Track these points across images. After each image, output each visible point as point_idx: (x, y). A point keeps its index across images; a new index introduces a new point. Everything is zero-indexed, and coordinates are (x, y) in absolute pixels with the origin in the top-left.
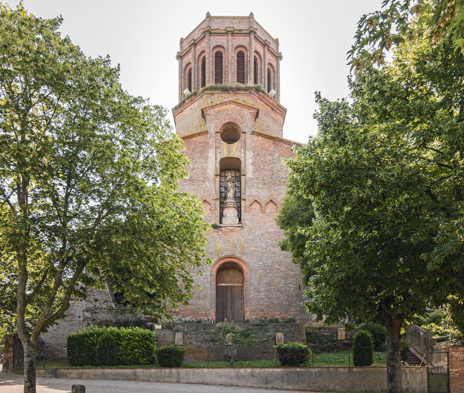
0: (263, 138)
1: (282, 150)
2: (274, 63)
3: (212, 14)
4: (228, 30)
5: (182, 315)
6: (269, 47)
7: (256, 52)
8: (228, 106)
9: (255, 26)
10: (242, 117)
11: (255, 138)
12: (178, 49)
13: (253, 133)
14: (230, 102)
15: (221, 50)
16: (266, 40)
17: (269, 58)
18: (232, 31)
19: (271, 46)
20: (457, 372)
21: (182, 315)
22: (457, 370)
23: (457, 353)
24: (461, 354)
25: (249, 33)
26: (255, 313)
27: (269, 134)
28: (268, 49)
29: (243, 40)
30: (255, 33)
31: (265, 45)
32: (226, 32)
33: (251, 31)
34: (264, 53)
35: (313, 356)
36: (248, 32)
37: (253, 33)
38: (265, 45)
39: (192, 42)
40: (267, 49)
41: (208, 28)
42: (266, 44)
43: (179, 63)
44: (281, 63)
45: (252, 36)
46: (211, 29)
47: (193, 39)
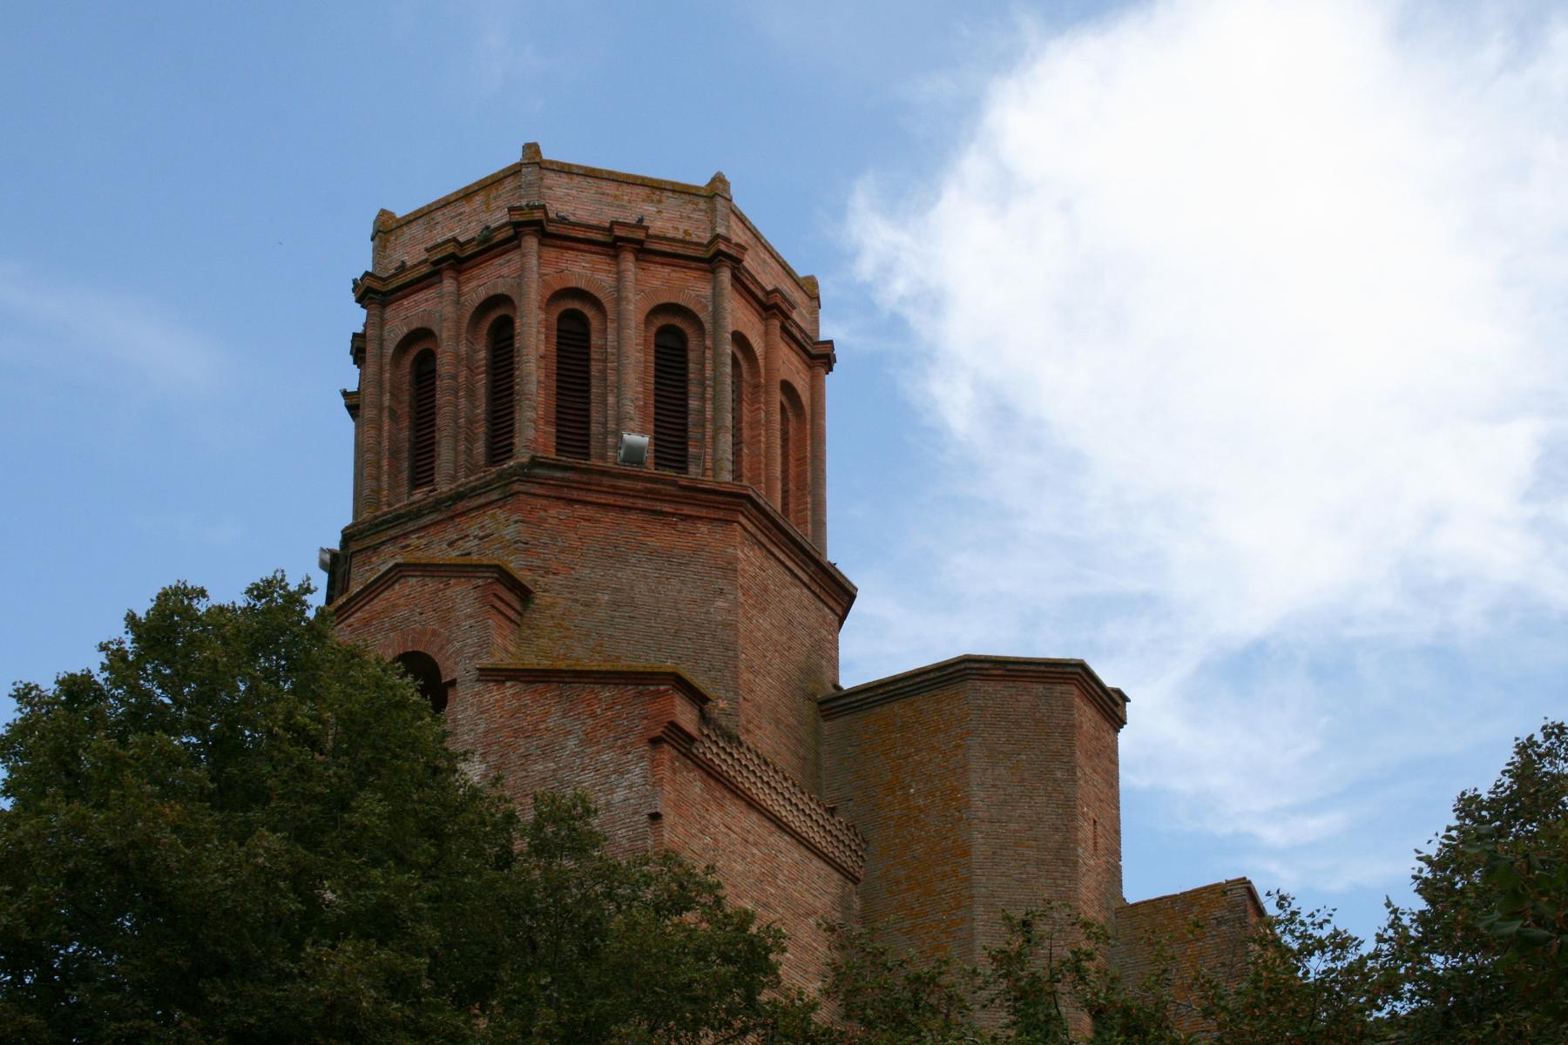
0: (519, 687)
1: (593, 715)
2: (801, 384)
3: (548, 154)
4: (618, 232)
6: (788, 317)
7: (740, 339)
8: (397, 587)
9: (739, 235)
11: (493, 694)
12: (362, 261)
13: (494, 675)
14: (399, 572)
15: (589, 312)
16: (776, 290)
17: (788, 364)
18: (640, 242)
19: (795, 316)
25: (709, 261)
28: (784, 329)
29: (691, 289)
31: (771, 307)
33: (720, 253)
34: (769, 348)
36: (708, 256)
37: (729, 263)
39: (450, 249)
40: (777, 323)
43: (697, 188)
44: (831, 381)
45: (725, 276)
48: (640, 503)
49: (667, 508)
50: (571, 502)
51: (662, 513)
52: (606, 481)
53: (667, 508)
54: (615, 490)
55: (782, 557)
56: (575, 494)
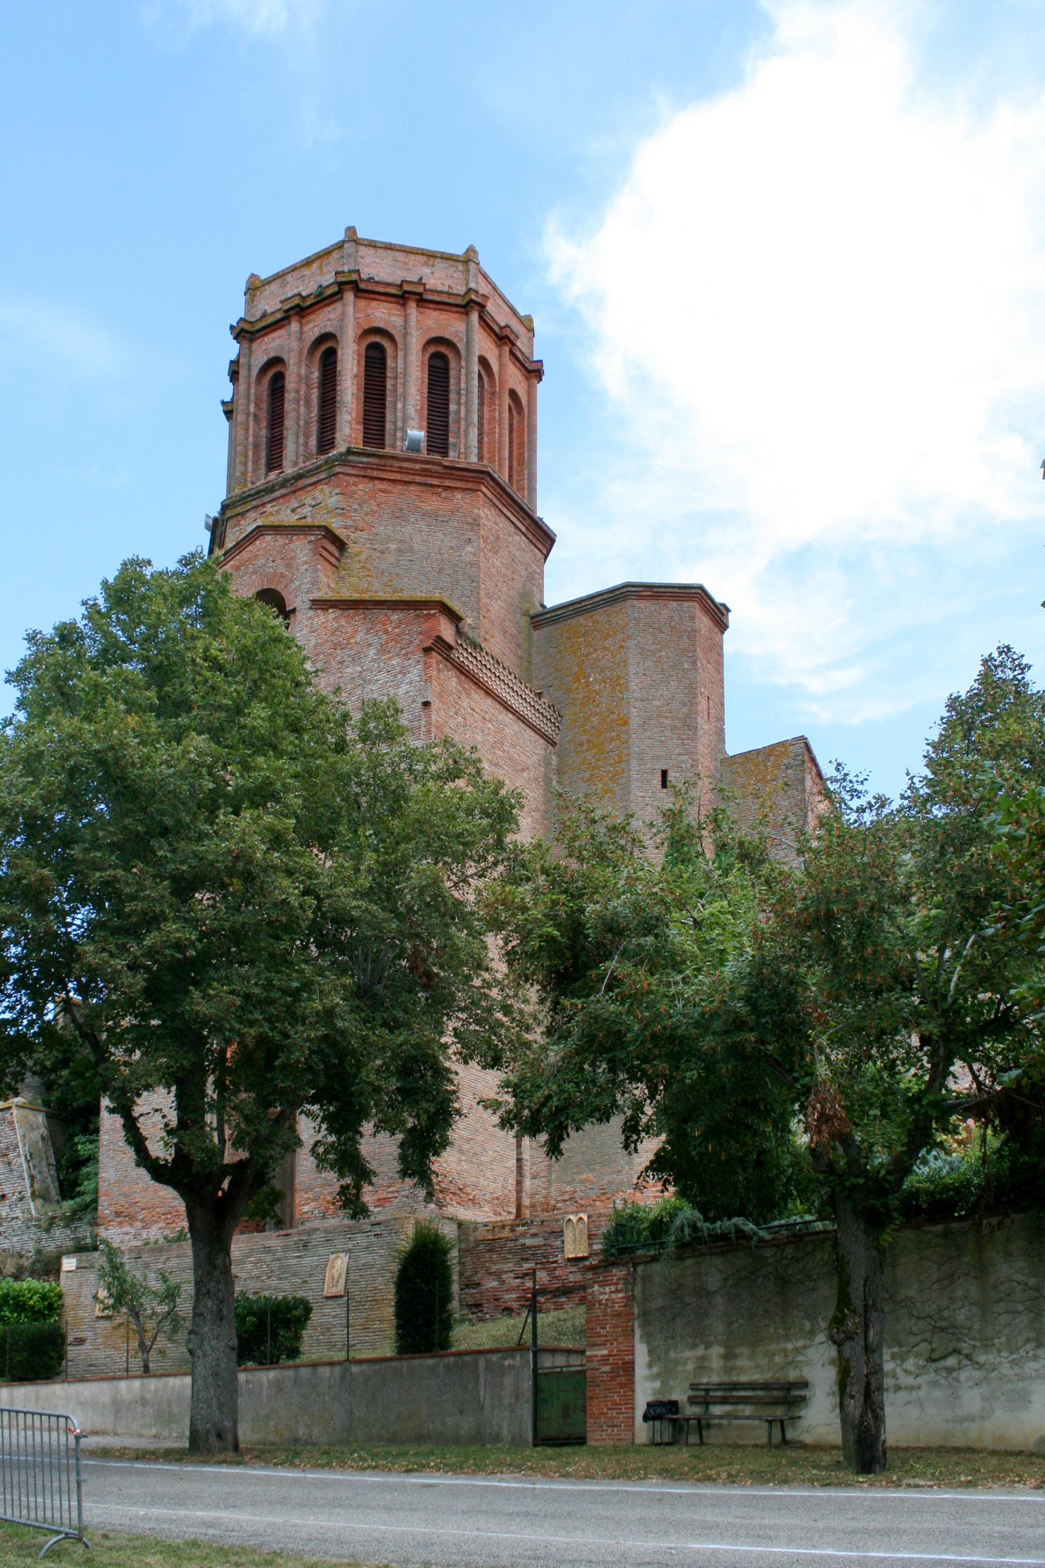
4: (406, 288)
5: (142, 1220)
6: (513, 344)
10: (289, 566)
11: (321, 618)
13: (321, 605)
16: (507, 326)
18: (420, 294)
19: (519, 343)
20: (605, 1359)
21: (142, 1220)
22: (605, 1352)
23: (607, 1289)
24: (617, 1291)
25: (464, 307)
26: (310, 1195)
27: (405, 596)
30: (482, 307)
31: (503, 338)
32: (400, 293)
33: (471, 301)
35: (314, 1365)
36: (463, 303)
37: (477, 308)
38: (503, 338)
39: (297, 301)
40: (507, 349)
41: (354, 277)
42: (507, 337)
45: (475, 317)
46: (361, 280)
47: (299, 295)
48: (418, 479)
49: (435, 482)
50: (373, 478)
51: (432, 486)
52: (396, 464)
53: (435, 482)
54: (401, 470)
55: (509, 514)
56: (375, 474)
